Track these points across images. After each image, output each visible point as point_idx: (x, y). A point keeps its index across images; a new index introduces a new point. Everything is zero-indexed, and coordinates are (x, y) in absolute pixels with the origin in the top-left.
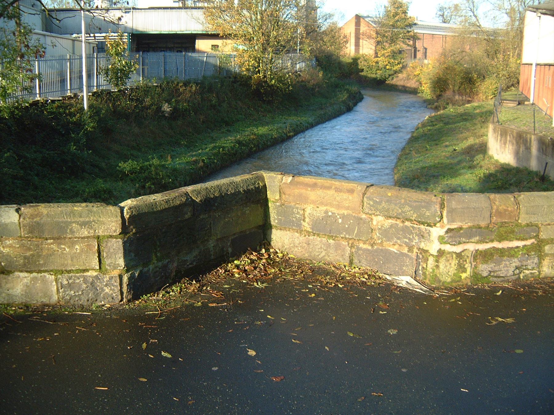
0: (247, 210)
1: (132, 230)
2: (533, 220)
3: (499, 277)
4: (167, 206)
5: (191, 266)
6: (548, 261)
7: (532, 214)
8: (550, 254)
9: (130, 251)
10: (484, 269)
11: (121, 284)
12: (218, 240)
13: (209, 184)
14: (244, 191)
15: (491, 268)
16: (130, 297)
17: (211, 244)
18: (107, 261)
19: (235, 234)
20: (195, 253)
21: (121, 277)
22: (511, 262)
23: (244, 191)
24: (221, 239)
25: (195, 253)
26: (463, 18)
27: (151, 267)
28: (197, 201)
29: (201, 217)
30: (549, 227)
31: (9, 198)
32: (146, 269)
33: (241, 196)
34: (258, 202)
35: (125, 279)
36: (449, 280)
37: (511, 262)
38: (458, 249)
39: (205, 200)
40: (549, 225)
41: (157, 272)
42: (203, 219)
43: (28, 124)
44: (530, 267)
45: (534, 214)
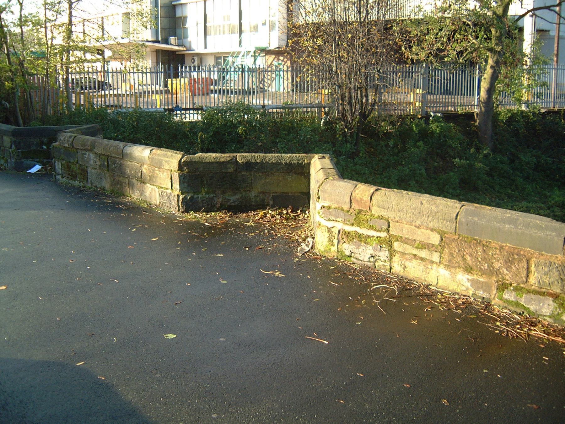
0: (289, 178)
1: (186, 170)
2: (383, 213)
3: (358, 260)
4: (213, 161)
5: (232, 204)
6: (398, 258)
7: (382, 208)
8: (428, 260)
9: (184, 182)
10: (347, 248)
11: (178, 200)
12: (259, 193)
13: (21, 119)
14: (286, 163)
15: (352, 249)
16: (183, 210)
17: (253, 194)
18: (174, 185)
19: (276, 193)
20: (238, 196)
21: (178, 196)
22: (367, 249)
23: (286, 163)
24: (263, 193)
25: (238, 196)
26: (448, 24)
27: (200, 196)
28: (240, 162)
29: (243, 173)
30: (397, 224)
31: (483, 192)
32: (196, 196)
33: (282, 166)
34: (302, 174)
35: (181, 198)
36: (323, 249)
37: (367, 249)
38: (330, 224)
39: (246, 163)
40: (398, 222)
41: (204, 200)
42: (244, 175)
43: (539, 130)
44: (382, 259)
45: (384, 209)
